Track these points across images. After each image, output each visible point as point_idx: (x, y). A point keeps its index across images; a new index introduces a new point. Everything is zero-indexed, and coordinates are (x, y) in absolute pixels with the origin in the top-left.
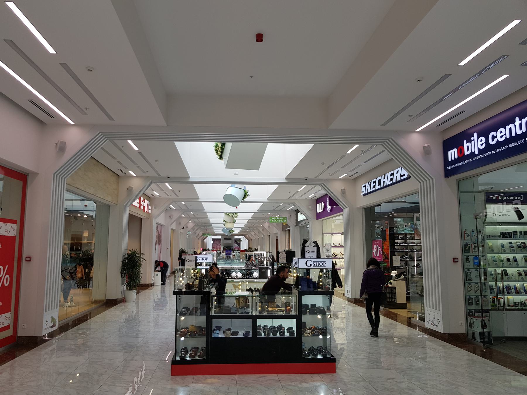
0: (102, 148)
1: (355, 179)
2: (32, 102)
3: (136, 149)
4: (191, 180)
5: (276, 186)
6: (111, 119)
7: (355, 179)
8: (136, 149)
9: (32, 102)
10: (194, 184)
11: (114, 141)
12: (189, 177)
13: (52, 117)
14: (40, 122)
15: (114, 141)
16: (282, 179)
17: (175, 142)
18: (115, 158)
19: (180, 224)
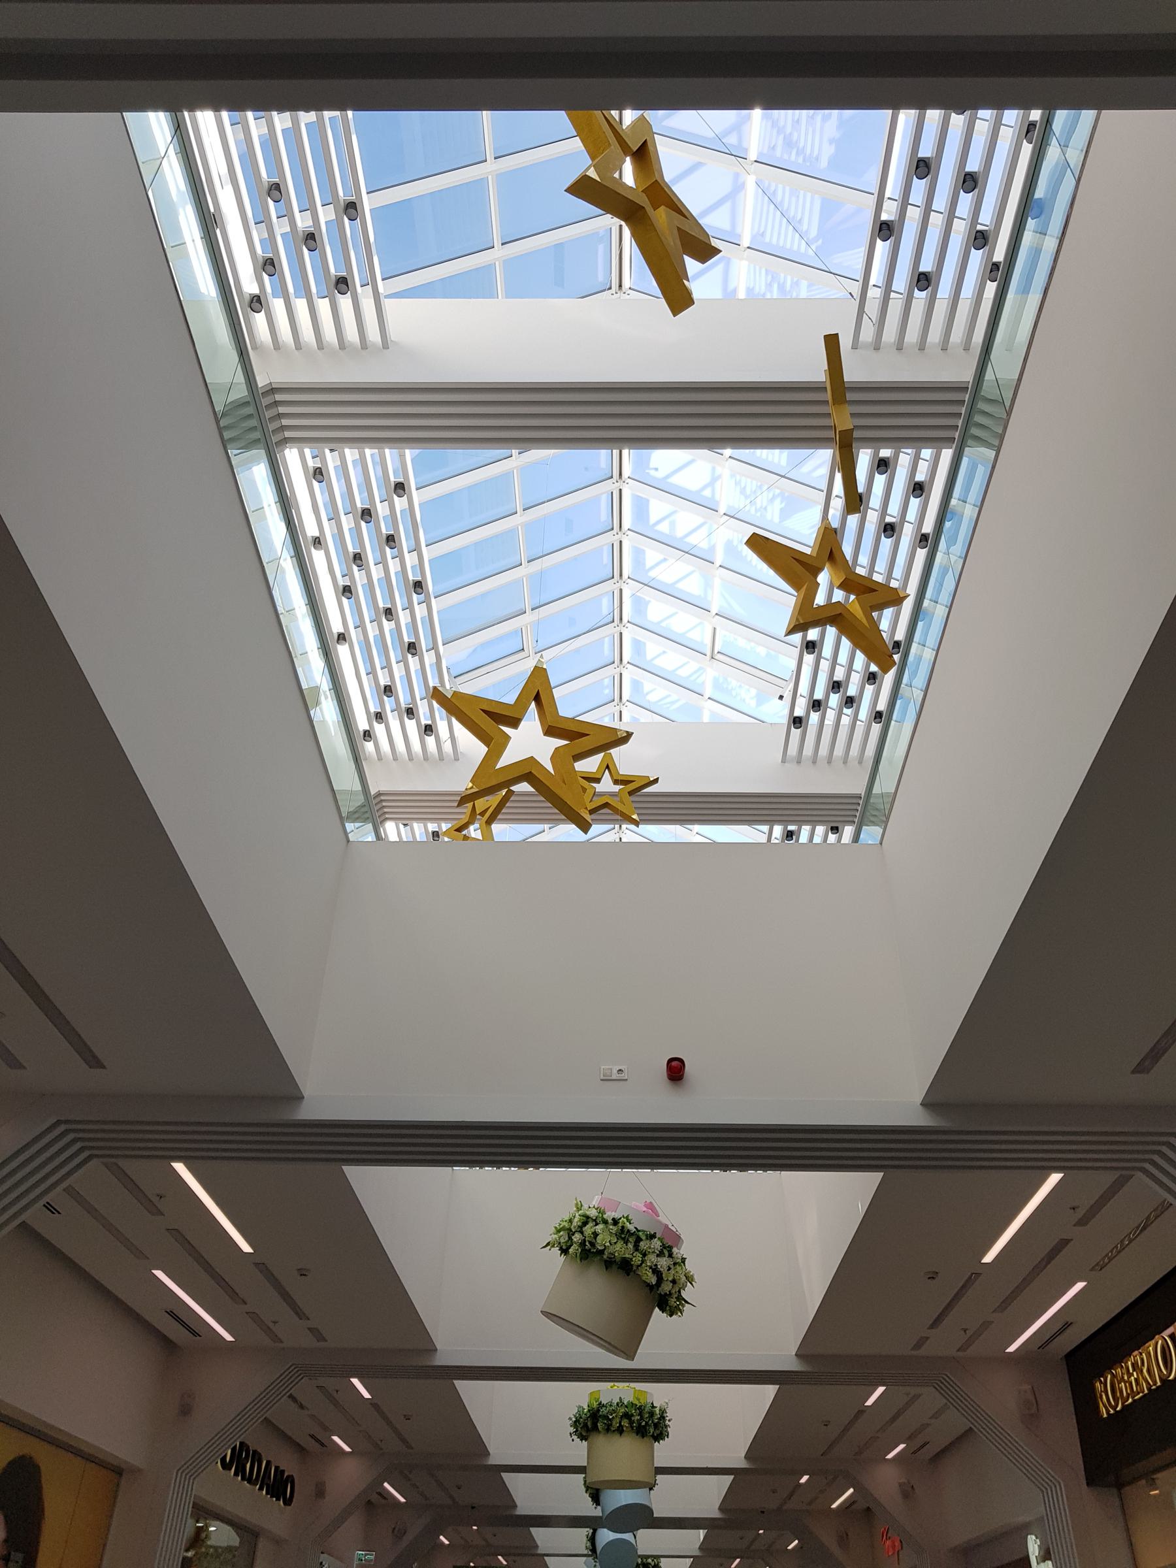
0: (69, 1190)
1: (938, 1457)
2: (171, 1314)
3: (367, 1395)
4: (440, 1360)
5: (771, 1391)
6: (94, 1062)
7: (938, 1457)
8: (367, 1395)
9: (171, 1314)
10: (459, 1384)
11: (121, 1163)
12: (301, 1098)
13: (195, 1333)
14: (168, 1344)
15: (121, 1163)
16: (896, 1093)
17: (532, 1529)
18: (313, 1417)
19: (185, 1411)
